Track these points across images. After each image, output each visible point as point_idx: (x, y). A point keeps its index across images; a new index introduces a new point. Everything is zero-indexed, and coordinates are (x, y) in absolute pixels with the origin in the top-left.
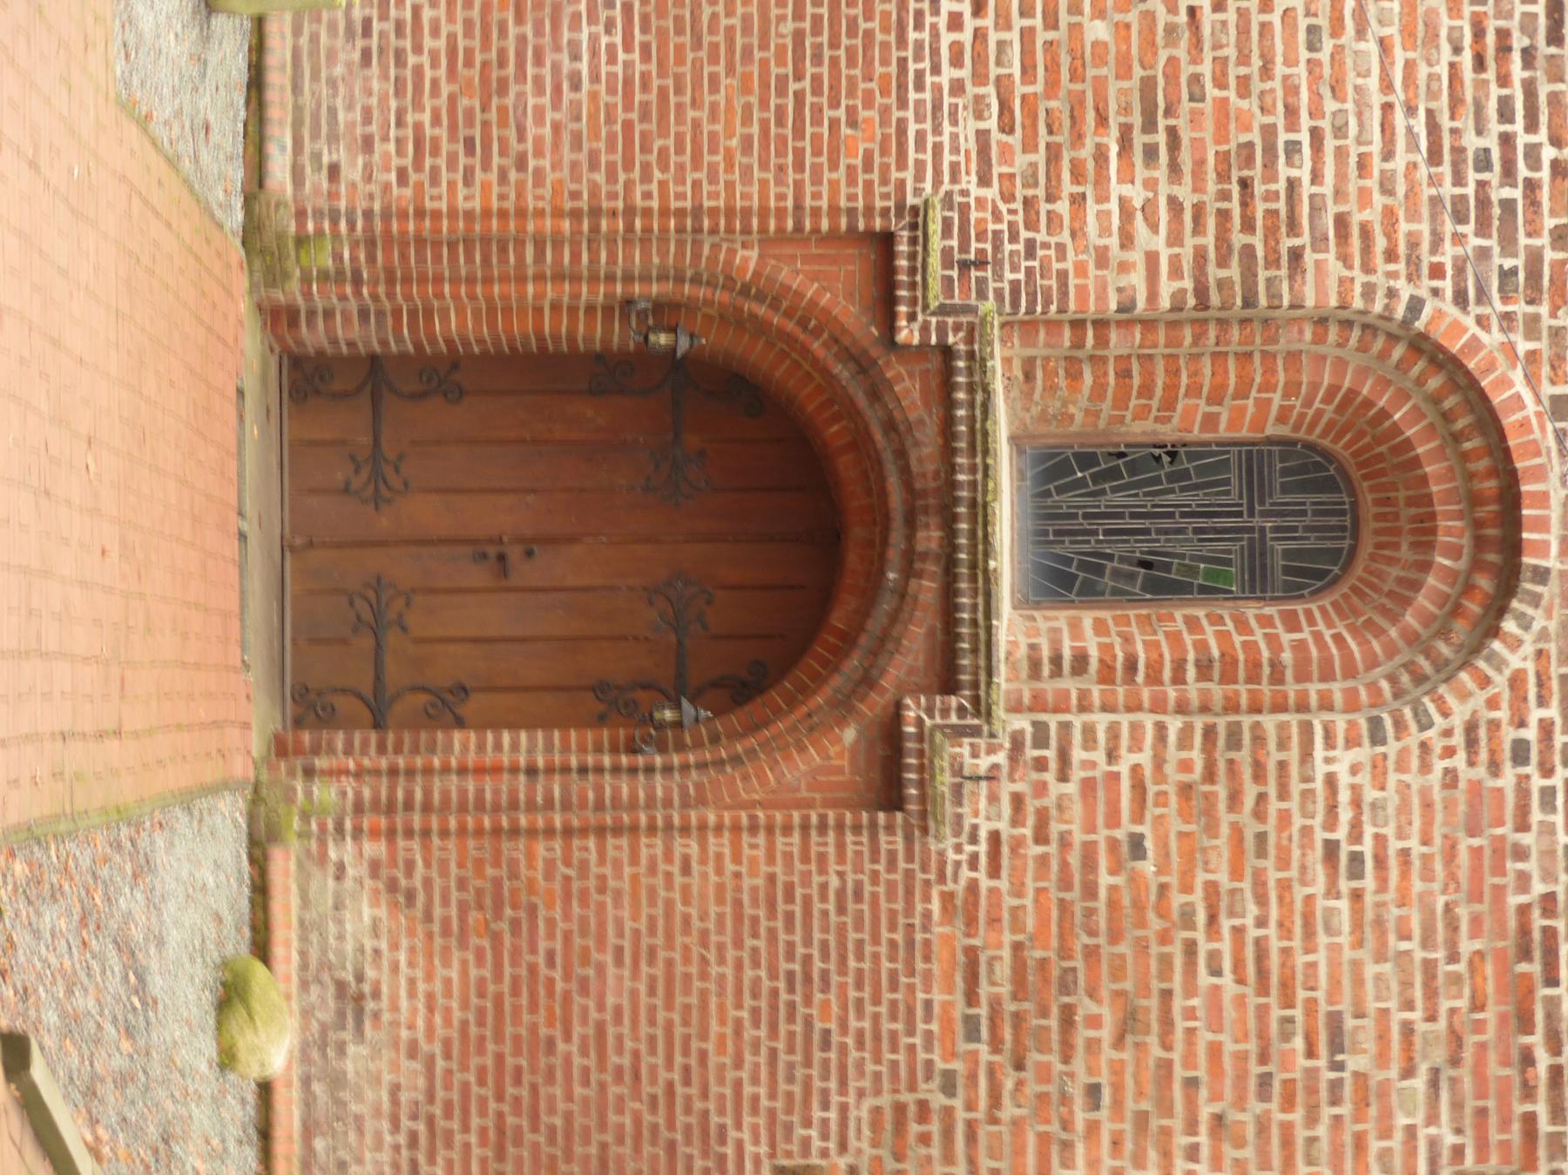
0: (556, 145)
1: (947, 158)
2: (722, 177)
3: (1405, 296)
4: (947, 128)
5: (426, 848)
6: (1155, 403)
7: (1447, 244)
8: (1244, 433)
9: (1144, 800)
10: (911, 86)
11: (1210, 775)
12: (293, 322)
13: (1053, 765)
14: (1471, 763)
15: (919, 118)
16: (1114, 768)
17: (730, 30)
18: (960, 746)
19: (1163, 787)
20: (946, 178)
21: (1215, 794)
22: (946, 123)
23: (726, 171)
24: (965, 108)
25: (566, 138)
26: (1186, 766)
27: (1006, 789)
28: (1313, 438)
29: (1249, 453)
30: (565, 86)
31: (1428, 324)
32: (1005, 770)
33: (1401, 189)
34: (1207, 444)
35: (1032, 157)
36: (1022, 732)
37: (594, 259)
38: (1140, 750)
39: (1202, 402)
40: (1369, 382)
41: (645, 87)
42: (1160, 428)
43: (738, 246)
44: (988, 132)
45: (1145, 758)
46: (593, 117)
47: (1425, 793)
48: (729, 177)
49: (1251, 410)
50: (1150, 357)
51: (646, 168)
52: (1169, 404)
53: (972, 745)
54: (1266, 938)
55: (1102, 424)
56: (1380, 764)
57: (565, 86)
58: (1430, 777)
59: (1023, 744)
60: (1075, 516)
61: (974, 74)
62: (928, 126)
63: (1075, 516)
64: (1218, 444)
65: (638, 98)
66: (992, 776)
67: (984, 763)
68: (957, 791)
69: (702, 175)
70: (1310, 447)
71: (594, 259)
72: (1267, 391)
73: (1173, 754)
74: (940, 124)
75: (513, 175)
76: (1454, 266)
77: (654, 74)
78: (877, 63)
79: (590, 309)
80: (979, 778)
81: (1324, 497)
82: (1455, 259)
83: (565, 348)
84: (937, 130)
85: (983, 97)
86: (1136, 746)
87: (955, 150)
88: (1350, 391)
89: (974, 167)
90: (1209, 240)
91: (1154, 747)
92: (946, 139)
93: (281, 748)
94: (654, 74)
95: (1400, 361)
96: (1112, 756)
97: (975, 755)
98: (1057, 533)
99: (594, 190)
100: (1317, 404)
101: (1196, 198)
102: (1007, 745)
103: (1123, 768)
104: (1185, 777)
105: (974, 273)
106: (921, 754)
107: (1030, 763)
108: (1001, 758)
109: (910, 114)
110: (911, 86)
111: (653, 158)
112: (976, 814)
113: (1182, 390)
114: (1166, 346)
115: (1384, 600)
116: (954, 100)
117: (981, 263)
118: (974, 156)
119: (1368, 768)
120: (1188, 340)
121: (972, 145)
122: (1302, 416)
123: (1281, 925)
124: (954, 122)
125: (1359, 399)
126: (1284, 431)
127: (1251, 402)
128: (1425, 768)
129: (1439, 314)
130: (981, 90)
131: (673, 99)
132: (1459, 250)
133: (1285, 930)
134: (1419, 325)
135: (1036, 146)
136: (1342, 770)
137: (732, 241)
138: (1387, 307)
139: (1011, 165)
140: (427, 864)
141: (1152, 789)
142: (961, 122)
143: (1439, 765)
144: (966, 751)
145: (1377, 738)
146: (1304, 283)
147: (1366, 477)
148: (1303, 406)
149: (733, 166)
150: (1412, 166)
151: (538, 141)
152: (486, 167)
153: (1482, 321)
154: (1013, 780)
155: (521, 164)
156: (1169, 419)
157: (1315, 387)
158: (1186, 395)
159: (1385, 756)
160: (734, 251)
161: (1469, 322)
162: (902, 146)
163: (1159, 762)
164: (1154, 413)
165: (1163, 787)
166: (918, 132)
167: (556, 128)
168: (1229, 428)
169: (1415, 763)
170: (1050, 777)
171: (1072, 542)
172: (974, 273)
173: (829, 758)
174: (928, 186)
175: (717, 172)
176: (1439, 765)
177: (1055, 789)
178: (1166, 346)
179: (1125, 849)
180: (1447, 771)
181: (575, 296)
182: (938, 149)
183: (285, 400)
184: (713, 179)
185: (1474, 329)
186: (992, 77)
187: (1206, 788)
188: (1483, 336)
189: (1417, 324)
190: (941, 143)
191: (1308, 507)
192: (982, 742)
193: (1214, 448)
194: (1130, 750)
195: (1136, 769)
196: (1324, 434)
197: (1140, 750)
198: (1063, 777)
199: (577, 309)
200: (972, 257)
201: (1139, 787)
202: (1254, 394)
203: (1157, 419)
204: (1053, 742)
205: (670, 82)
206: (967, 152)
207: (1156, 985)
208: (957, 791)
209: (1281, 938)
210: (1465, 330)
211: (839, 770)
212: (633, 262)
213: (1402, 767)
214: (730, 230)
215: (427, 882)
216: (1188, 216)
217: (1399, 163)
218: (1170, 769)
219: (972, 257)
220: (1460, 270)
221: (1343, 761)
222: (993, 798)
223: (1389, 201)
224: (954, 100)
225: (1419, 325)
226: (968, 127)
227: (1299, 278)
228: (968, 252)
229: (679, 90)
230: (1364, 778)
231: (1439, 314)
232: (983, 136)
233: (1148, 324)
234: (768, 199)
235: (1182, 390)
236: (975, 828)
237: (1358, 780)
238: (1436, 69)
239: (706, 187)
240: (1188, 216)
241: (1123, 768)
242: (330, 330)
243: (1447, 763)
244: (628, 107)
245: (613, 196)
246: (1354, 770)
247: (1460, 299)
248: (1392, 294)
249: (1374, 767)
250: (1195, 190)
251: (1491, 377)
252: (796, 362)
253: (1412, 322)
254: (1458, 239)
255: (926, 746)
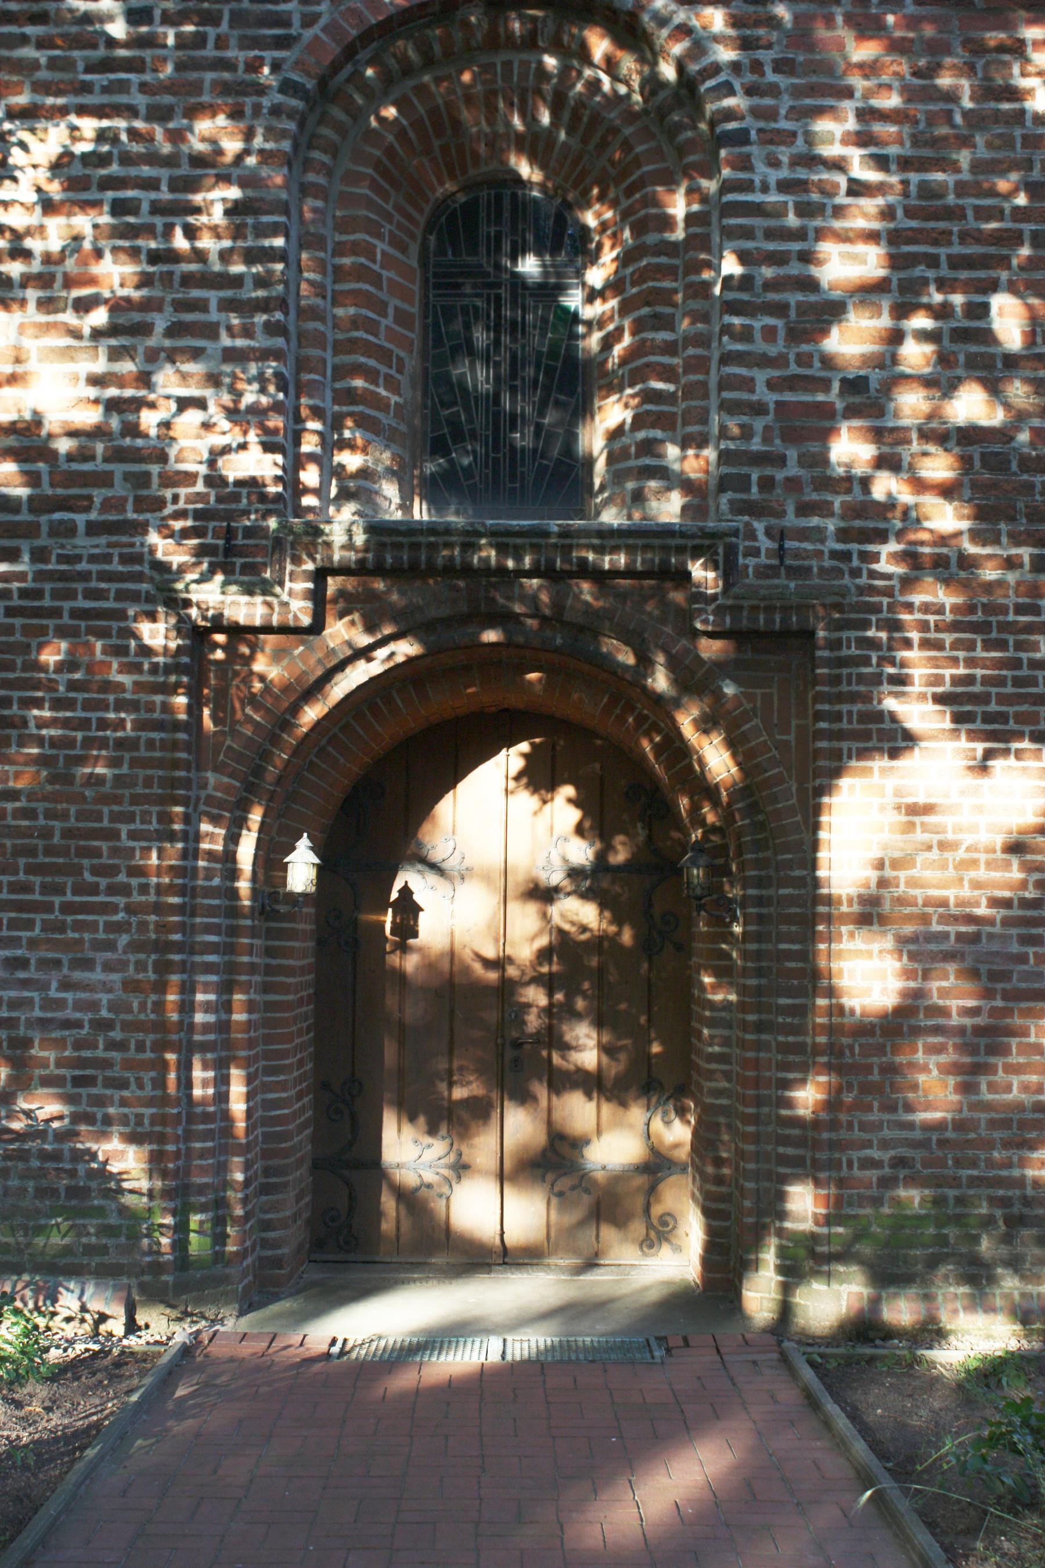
0: (87, 987)
1: (116, 566)
2: (127, 808)
3: (279, 98)
4: (83, 566)
5: (852, 1145)
6: (383, 369)
7: (230, 54)
8: (416, 288)
9: (806, 377)
10: (36, 604)
11: (780, 309)
12: (277, 1262)
13: (768, 471)
14: (769, 46)
15: (71, 595)
16: (772, 406)
17: (115, 835)
18: (747, 567)
19: (792, 357)
20: (137, 568)
21: (799, 305)
22: (79, 567)
23: (120, 803)
24: (63, 547)
25: (78, 975)
26: (770, 333)
27: (791, 519)
28: (422, 220)
29: (437, 286)
30: (22, 975)
31: (308, 74)
32: (773, 521)
33: (167, 99)
34: (425, 328)
35: (118, 478)
36: (731, 502)
37: (212, 948)
38: (752, 379)
39: (384, 322)
40: (368, 149)
41: (26, 888)
42: (408, 369)
43: (203, 794)
44: (89, 523)
45: (761, 376)
46: (55, 945)
47: (798, 92)
48: (126, 799)
49: (392, 274)
50: (335, 368)
51: (112, 890)
52: (385, 356)
53: (745, 556)
54: (949, 257)
55: (403, 428)
56: (768, 136)
57: (22, 975)
58: (782, 86)
59: (745, 501)
60: (496, 461)
61: (26, 536)
62: (80, 586)
63: (496, 461)
64: (426, 317)
65: (37, 897)
66: (780, 535)
67: (765, 543)
68: (796, 572)
69: (124, 829)
70: (429, 228)
71: (212, 948)
72: (374, 254)
73: (760, 346)
74: (79, 573)
75: (116, 1035)
76: (251, 48)
77: (12, 879)
78: (12, 639)
79: (270, 952)
80: (781, 547)
81: (483, 214)
82: (242, 47)
83: (311, 977)
84: (85, 576)
85: (51, 528)
86: (748, 384)
87: (107, 558)
88: (376, 168)
89: (124, 539)
90: (213, 296)
91: (749, 366)
92: (94, 568)
93: (588, 1142)
94: (12, 879)
95: (347, 112)
96: (758, 409)
97: (755, 552)
98: (513, 478)
99: (135, 946)
100: (389, 207)
101: (169, 309)
102: (746, 518)
103: (771, 398)
104: (781, 334)
105: (240, 541)
106: (755, 609)
107: (765, 496)
108: (759, 526)
109: (67, 605)
110: (36, 604)
111: (103, 882)
112: (819, 554)
113: (371, 338)
114: (324, 349)
115: (591, 147)
116: (54, 558)
117: (230, 534)
118: (114, 539)
119: (772, 148)
120: (318, 325)
121: (103, 540)
122: (400, 226)
123: (936, 243)
124: (78, 558)
125: (385, 160)
126: (414, 248)
127: (385, 273)
128: (773, 90)
129: (298, 64)
130: (45, 529)
131: (41, 859)
132: (233, 42)
133: (942, 238)
134: (310, 84)
135: (105, 472)
136: (774, 176)
137: (198, 799)
138: (290, 117)
139: (125, 500)
140: (868, 1144)
141: (794, 369)
142: (77, 551)
143: (771, 77)
144: (751, 561)
145: (741, 138)
146: (262, 200)
147: (464, 171)
148: (390, 222)
149: (116, 796)
150: (144, 87)
151: (78, 1006)
152: (107, 1064)
153: (309, 21)
154: (782, 514)
155: (105, 1025)
156: (398, 358)
157: (370, 204)
158: (376, 336)
159: (760, 131)
160: (209, 797)
161: (308, 34)
162: (99, 614)
163: (765, 361)
164: (393, 372)
165: (792, 357)
166: (85, 597)
167: (66, 985)
168: (412, 304)
169: (768, 101)
170: (780, 475)
171: (523, 465)
172: (240, 541)
173: (754, 709)
174: (145, 586)
175: (120, 813)
176: (771, 77)
177: (793, 470)
178: (324, 349)
179: (857, 399)
180: (776, 70)
181: (252, 969)
182: (104, 576)
183: (351, 1257)
184: (130, 818)
185: (316, 30)
186: (30, 518)
187: (793, 314)
188: (323, 21)
189: (309, 86)
190: (99, 572)
191: (493, 230)
192: (742, 545)
193: (430, 320)
194: (752, 391)
195: (771, 385)
196: (421, 211)
197: (752, 379)
198: (781, 461)
199: (267, 966)
200: (221, 542)
201: (792, 383)
202: (376, 267)
203: (400, 371)
204: (744, 470)
205: (22, 861)
206: (109, 545)
207: (35, 1163)
208: (796, 572)
209: (950, 243)
210: (316, 38)
211: (767, 699)
212: (219, 907)
213: (771, 114)
214: (755, 1120)
215: (884, 1145)
216: (189, 317)
217: (140, 100)
218: (773, 350)
219: (221, 542)
220: (256, 43)
221: (761, 171)
222: (804, 534)
223: (179, 111)
224: (54, 558)
225: (310, 84)
226: (82, 543)
227: (257, 205)
228: (216, 546)
229: (32, 852)
230: (784, 154)
231: (298, 64)
232: (93, 529)
233: (302, 365)
234: (151, 758)
235: (371, 338)
236: (834, 554)
237: (785, 159)
238: (43, 61)
239: (137, 826)
240: (189, 317)
241: (771, 398)
242: (283, 1224)
243: (768, 69)
244: (48, 908)
245: (143, 926)
246: (774, 163)
247: (283, 42)
248: (276, 111)
249: (771, 142)
250: (160, 309)
251: (367, 13)
252: (329, 742)
253: (307, 92)
254: (221, 43)
255: (746, 603)
